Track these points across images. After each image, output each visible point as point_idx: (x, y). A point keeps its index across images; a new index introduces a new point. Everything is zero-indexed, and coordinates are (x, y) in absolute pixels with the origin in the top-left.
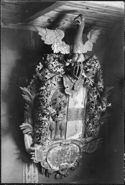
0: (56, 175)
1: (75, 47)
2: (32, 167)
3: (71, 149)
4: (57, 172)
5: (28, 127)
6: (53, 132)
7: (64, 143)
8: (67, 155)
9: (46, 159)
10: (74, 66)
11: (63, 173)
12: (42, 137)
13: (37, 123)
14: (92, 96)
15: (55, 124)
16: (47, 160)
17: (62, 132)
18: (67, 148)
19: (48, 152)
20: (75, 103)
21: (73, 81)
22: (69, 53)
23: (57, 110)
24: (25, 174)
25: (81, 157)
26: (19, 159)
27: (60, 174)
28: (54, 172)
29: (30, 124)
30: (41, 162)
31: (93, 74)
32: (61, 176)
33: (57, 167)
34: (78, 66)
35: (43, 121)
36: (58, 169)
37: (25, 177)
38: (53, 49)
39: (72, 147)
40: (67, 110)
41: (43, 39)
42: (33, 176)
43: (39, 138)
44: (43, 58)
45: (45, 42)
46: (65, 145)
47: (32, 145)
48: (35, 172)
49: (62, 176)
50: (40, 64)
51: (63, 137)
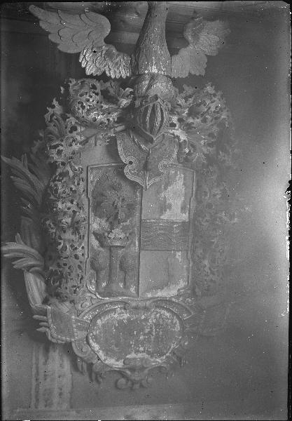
0: (117, 381)
1: (142, 59)
2: (55, 355)
3: (154, 321)
4: (120, 373)
5: (28, 254)
6: (103, 273)
7: (134, 304)
8: (145, 334)
9: (87, 337)
10: (142, 105)
11: (136, 377)
12: (64, 281)
13: (49, 250)
14: (207, 190)
15: (108, 254)
16: (91, 341)
17: (128, 277)
18: (143, 317)
19: (91, 320)
20: (164, 207)
21: (143, 146)
22: (128, 75)
23: (111, 220)
24: (37, 368)
25: (186, 344)
26: (20, 332)
27: (128, 379)
28: (109, 371)
29: (36, 249)
30: (73, 345)
31: (211, 135)
32: (130, 383)
33: (117, 360)
34: (151, 105)
35: (62, 242)
36: (119, 364)
37: (37, 373)
38: (83, 66)
39: (158, 315)
40: (138, 224)
41: (52, 38)
42: (57, 375)
43: (58, 283)
44: (62, 88)
45: (60, 48)
46: (136, 308)
47: (45, 301)
48: (63, 368)
49: (133, 384)
50: (55, 103)
51: (133, 290)
